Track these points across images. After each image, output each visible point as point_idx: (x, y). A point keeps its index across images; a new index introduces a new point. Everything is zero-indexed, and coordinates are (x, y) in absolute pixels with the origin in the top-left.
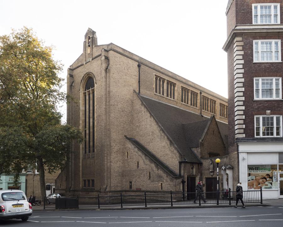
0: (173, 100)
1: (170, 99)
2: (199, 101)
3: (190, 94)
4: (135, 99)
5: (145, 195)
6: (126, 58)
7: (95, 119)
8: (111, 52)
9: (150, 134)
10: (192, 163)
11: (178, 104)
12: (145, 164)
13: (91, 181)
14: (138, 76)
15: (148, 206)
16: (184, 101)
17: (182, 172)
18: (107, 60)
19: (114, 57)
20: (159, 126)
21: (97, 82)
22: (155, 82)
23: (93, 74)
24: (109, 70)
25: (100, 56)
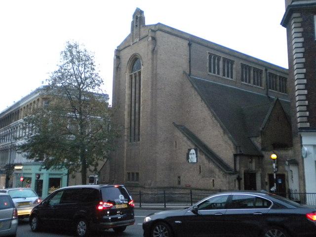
0: (231, 79)
1: (227, 78)
2: (264, 79)
3: (252, 72)
5: (191, 193)
6: (175, 37)
9: (202, 120)
10: (251, 156)
13: (135, 175)
17: (238, 166)
20: (212, 112)
21: (144, 64)
24: (157, 51)
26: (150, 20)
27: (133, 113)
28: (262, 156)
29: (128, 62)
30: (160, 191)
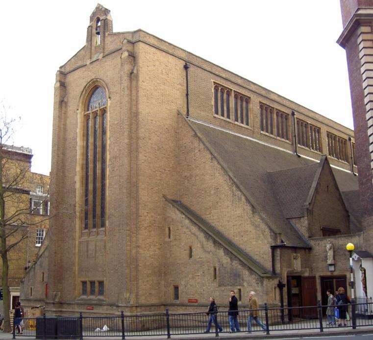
4: (180, 125)
6: (164, 53)
7: (108, 163)
8: (141, 45)
9: (212, 192)
11: (254, 135)
12: (205, 251)
13: (97, 284)
14: (185, 85)
15: (271, 333)
16: (265, 128)
18: (132, 58)
19: (144, 53)
21: (112, 96)
22: (213, 95)
23: (104, 81)
24: (137, 76)
25: (119, 52)
26: (120, 24)
27: (91, 179)
28: (310, 249)
29: (80, 93)
30: (146, 310)
